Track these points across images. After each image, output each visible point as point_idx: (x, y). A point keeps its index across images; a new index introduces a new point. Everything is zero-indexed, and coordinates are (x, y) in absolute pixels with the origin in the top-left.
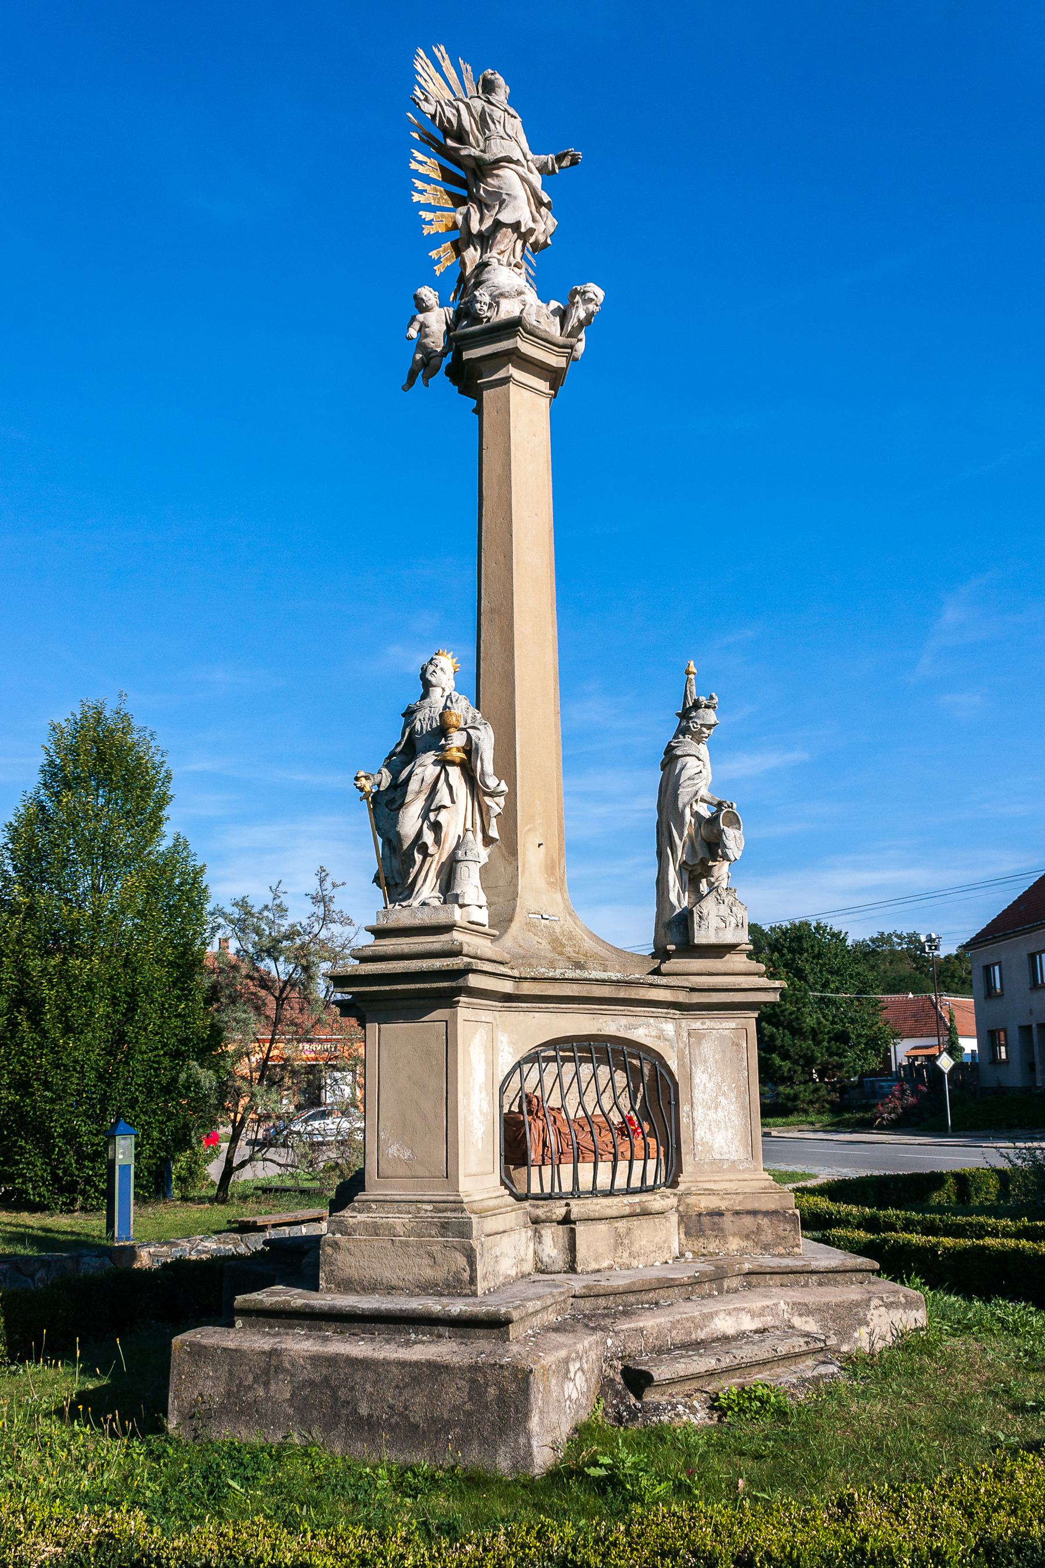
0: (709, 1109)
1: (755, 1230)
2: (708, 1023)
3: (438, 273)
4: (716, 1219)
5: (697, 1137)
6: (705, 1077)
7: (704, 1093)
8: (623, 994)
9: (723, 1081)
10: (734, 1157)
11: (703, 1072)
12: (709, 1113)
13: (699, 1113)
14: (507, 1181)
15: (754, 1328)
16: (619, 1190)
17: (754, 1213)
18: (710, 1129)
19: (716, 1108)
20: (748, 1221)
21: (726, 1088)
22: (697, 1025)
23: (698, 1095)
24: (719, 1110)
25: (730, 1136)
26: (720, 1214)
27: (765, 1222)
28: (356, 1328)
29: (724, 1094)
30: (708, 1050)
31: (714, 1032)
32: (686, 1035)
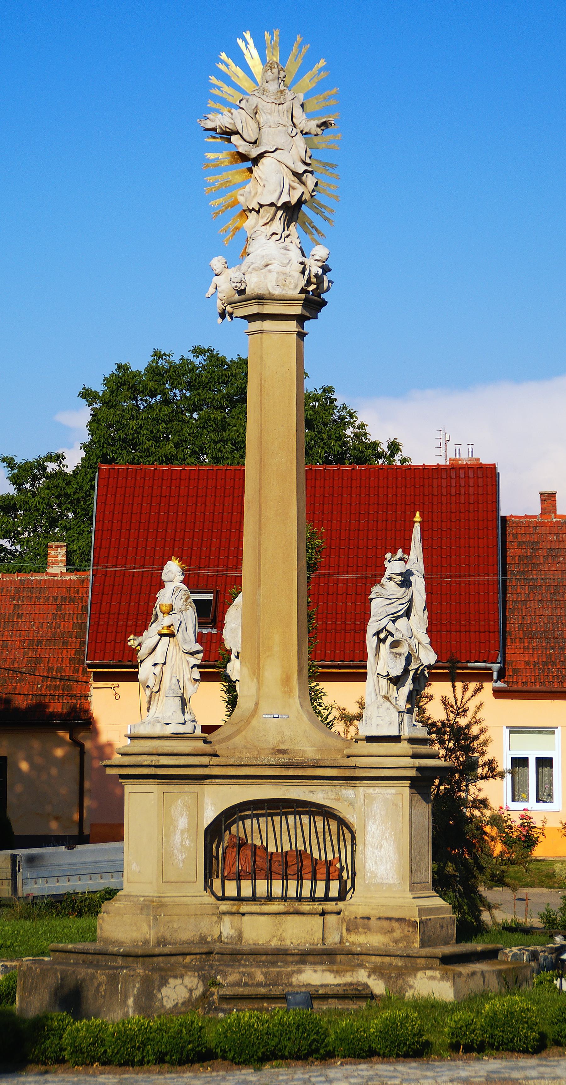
0: (376, 848)
1: (390, 930)
2: (377, 790)
3: (298, 36)
4: (366, 921)
5: (367, 867)
6: (375, 826)
7: (373, 837)
8: (291, 772)
9: (386, 830)
10: (390, 881)
11: (373, 824)
12: (376, 851)
13: (369, 851)
14: (208, 886)
15: (335, 983)
16: (319, 898)
17: (390, 919)
18: (376, 862)
19: (380, 848)
20: (385, 924)
21: (387, 835)
22: (371, 791)
23: (369, 839)
24: (383, 850)
25: (388, 867)
26: (369, 918)
27: (395, 925)
28: (276, 1000)
29: (386, 839)
30: (378, 809)
31: (381, 796)
32: (362, 797)
